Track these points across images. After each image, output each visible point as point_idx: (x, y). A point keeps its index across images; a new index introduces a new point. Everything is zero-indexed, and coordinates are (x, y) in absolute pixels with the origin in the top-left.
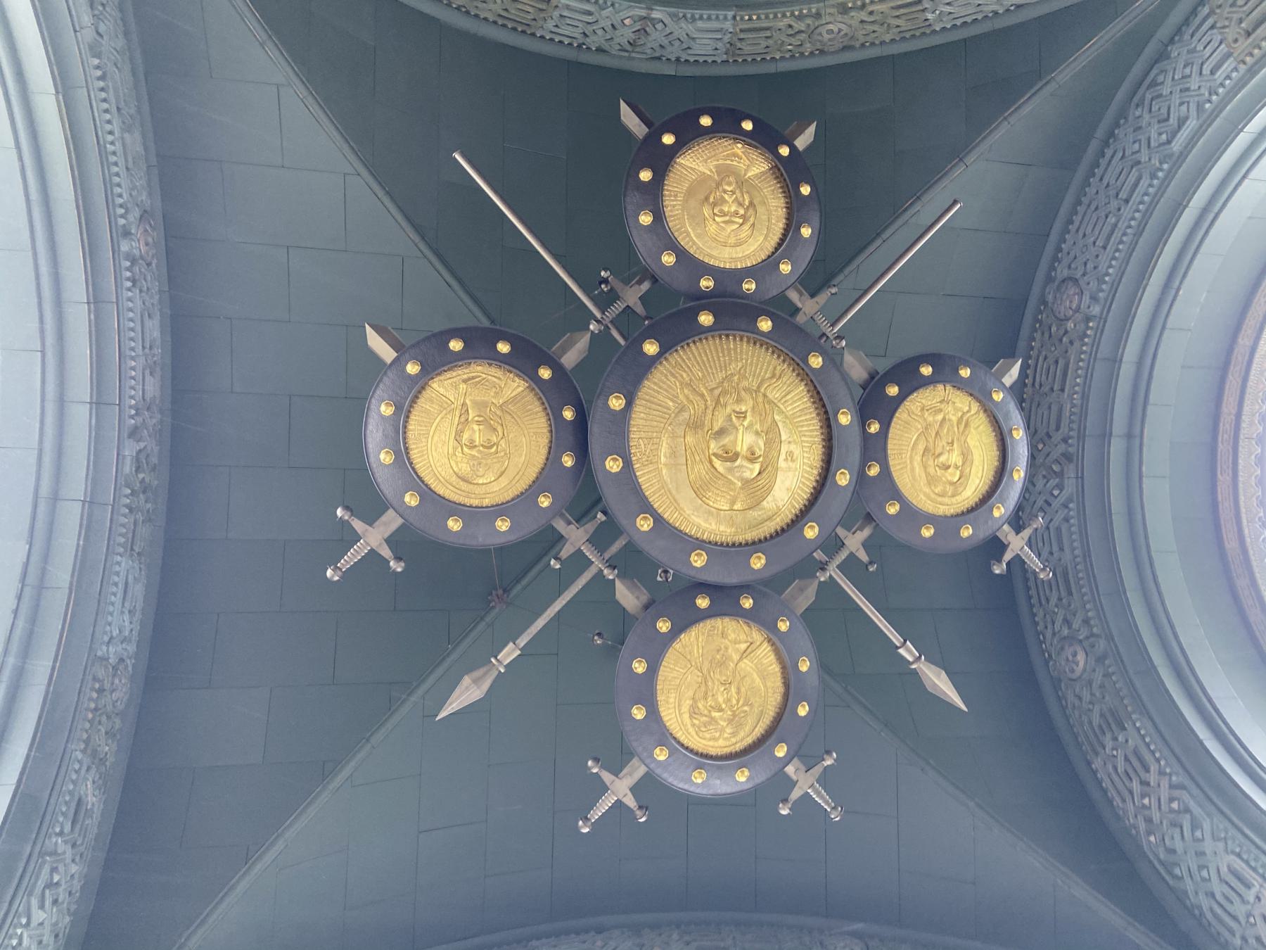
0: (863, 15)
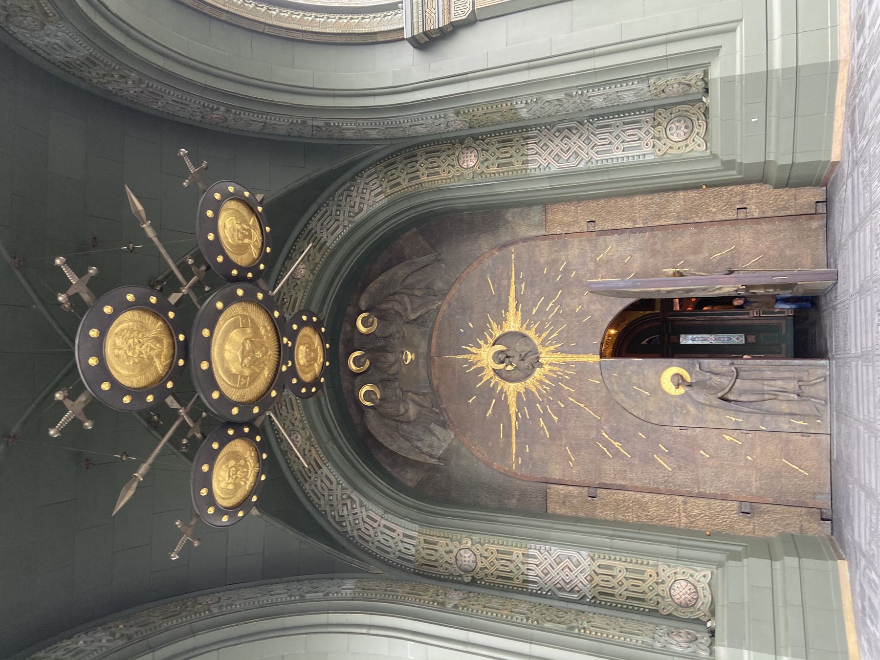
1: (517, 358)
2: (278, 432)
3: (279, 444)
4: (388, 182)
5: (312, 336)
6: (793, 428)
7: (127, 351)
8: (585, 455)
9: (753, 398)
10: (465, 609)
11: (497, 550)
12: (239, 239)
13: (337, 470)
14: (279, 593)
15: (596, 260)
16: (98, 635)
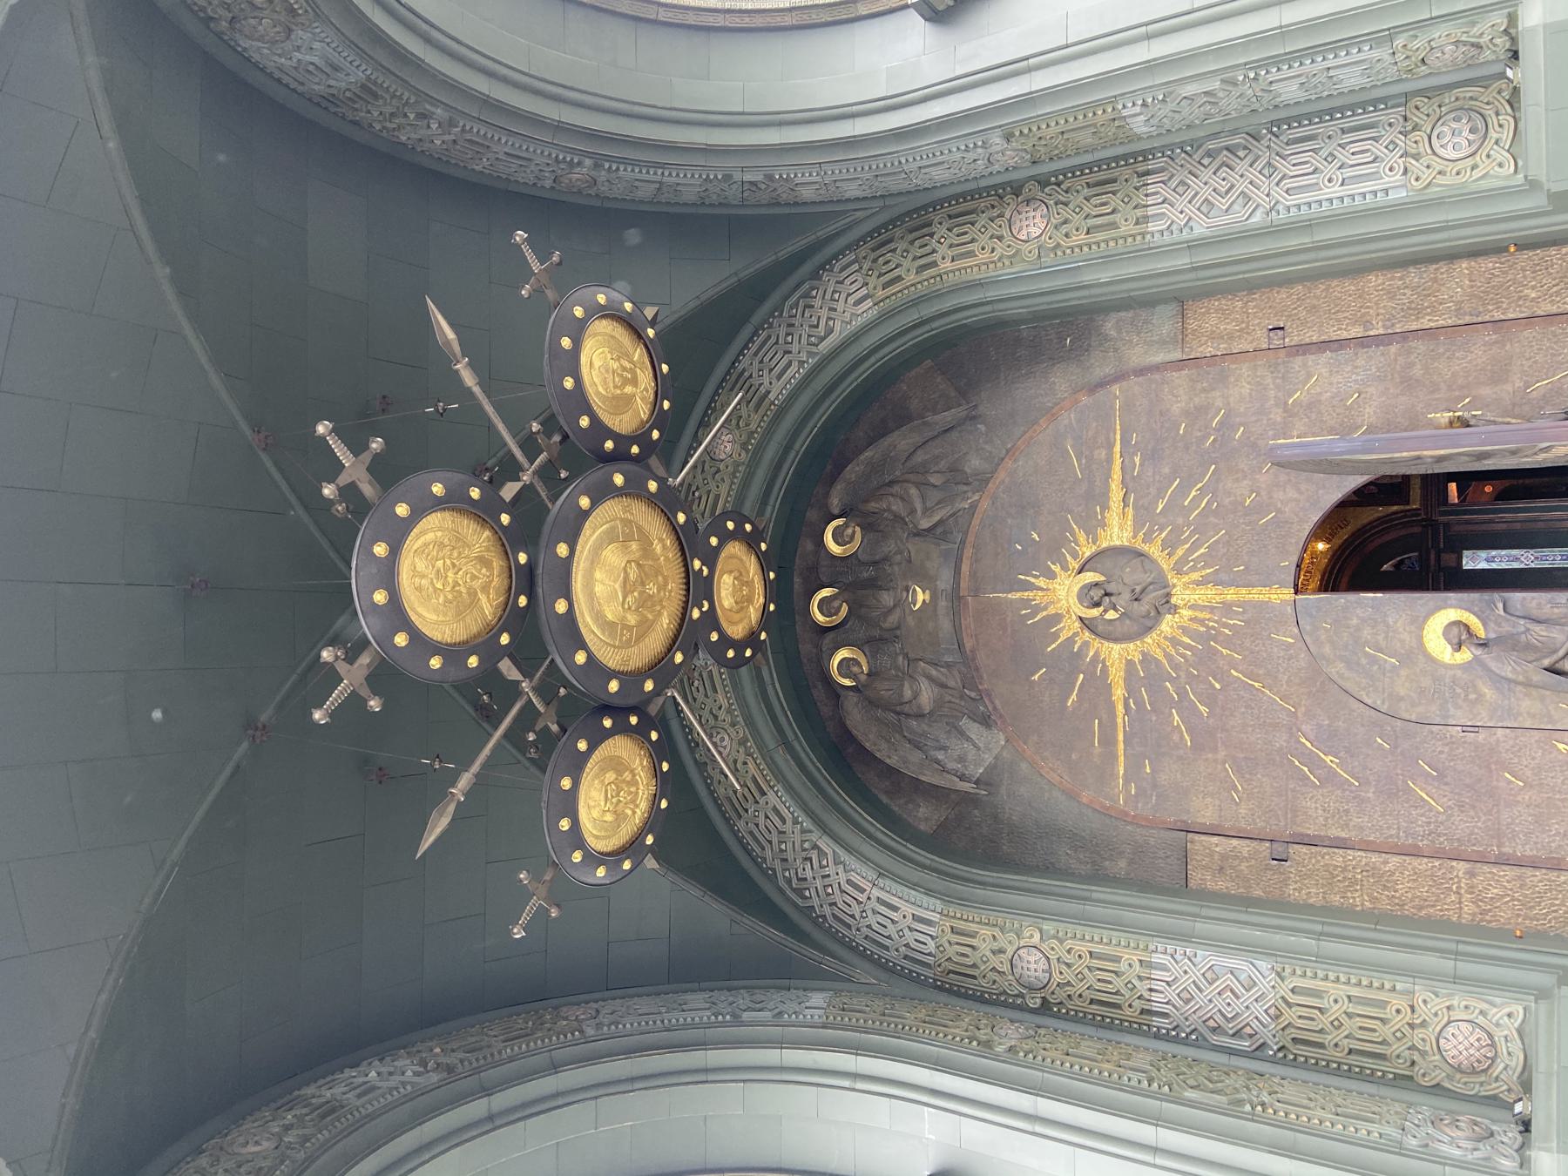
1: (1127, 596)
2: (691, 730)
3: (692, 751)
4: (879, 277)
5: (744, 558)
7: (435, 581)
11: (1090, 953)
12: (616, 387)
13: (792, 798)
14: (697, 1007)
15: (1286, 403)
16: (398, 1063)
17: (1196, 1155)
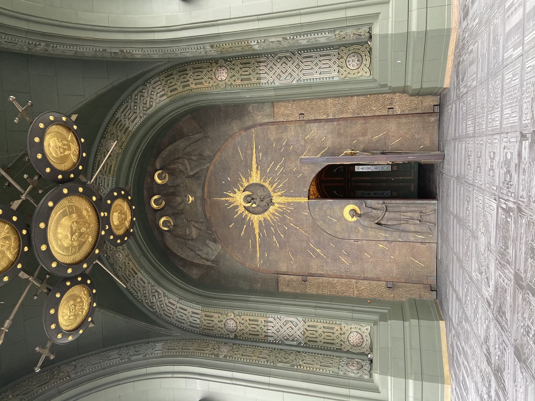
0: (127, 261)
1: (259, 200)
6: (417, 240)
8: (300, 257)
9: (395, 223)
10: (231, 358)
11: (249, 319)
15: (305, 139)
17: (294, 17)
